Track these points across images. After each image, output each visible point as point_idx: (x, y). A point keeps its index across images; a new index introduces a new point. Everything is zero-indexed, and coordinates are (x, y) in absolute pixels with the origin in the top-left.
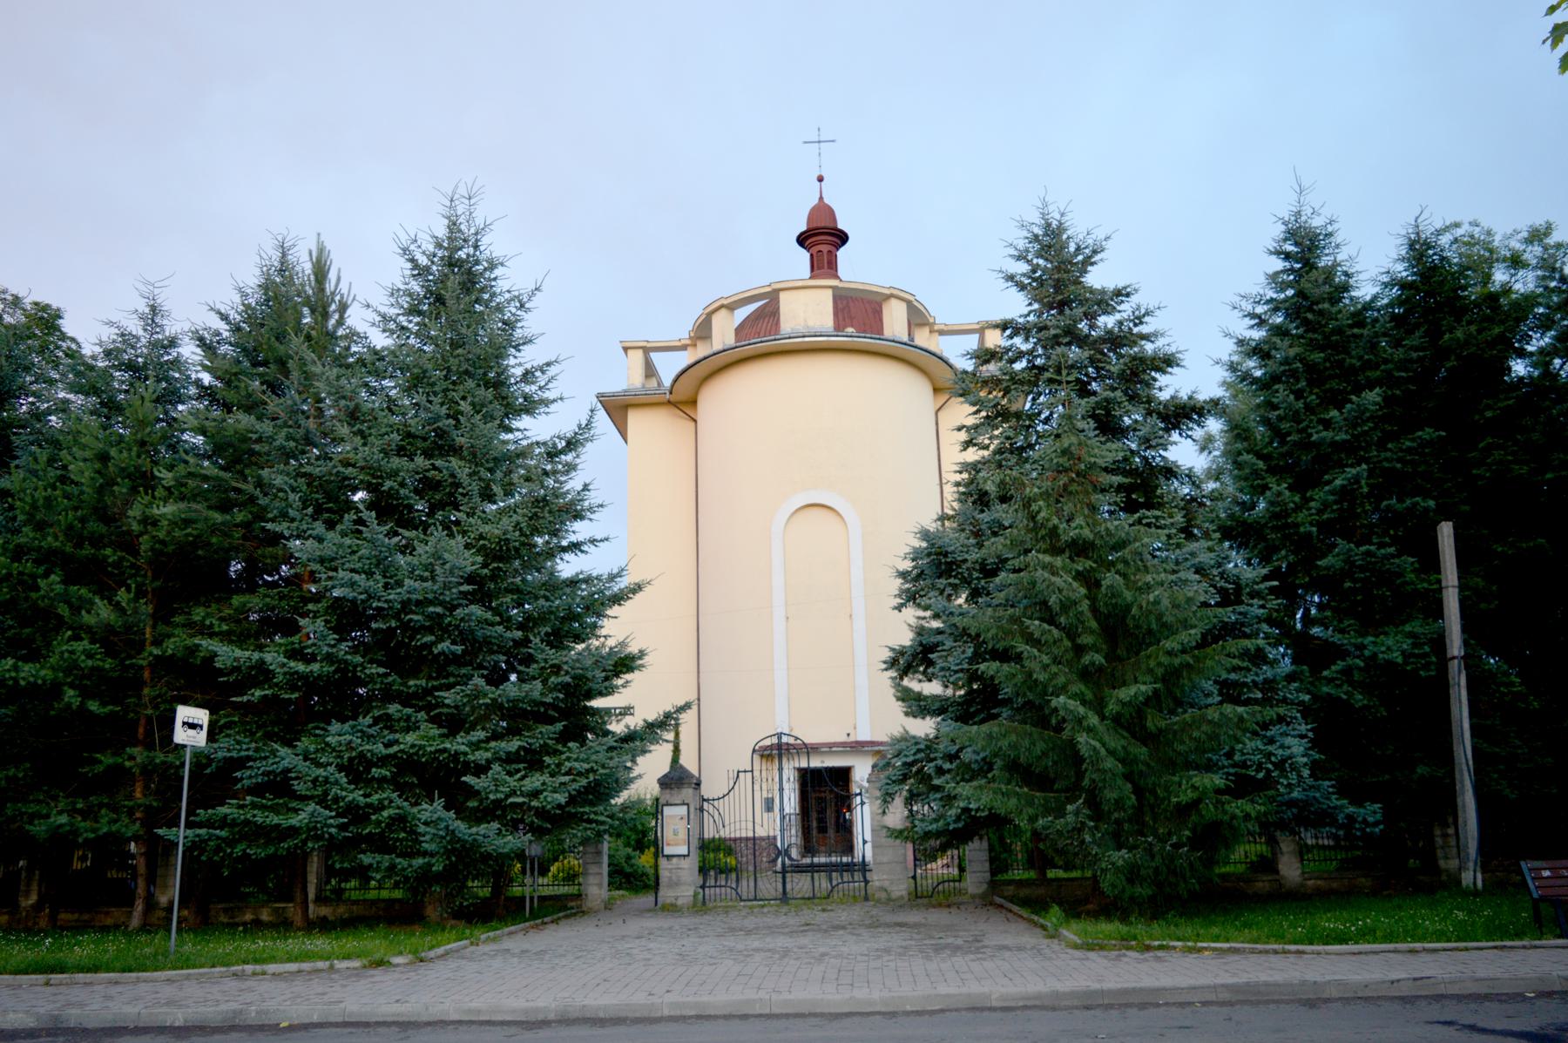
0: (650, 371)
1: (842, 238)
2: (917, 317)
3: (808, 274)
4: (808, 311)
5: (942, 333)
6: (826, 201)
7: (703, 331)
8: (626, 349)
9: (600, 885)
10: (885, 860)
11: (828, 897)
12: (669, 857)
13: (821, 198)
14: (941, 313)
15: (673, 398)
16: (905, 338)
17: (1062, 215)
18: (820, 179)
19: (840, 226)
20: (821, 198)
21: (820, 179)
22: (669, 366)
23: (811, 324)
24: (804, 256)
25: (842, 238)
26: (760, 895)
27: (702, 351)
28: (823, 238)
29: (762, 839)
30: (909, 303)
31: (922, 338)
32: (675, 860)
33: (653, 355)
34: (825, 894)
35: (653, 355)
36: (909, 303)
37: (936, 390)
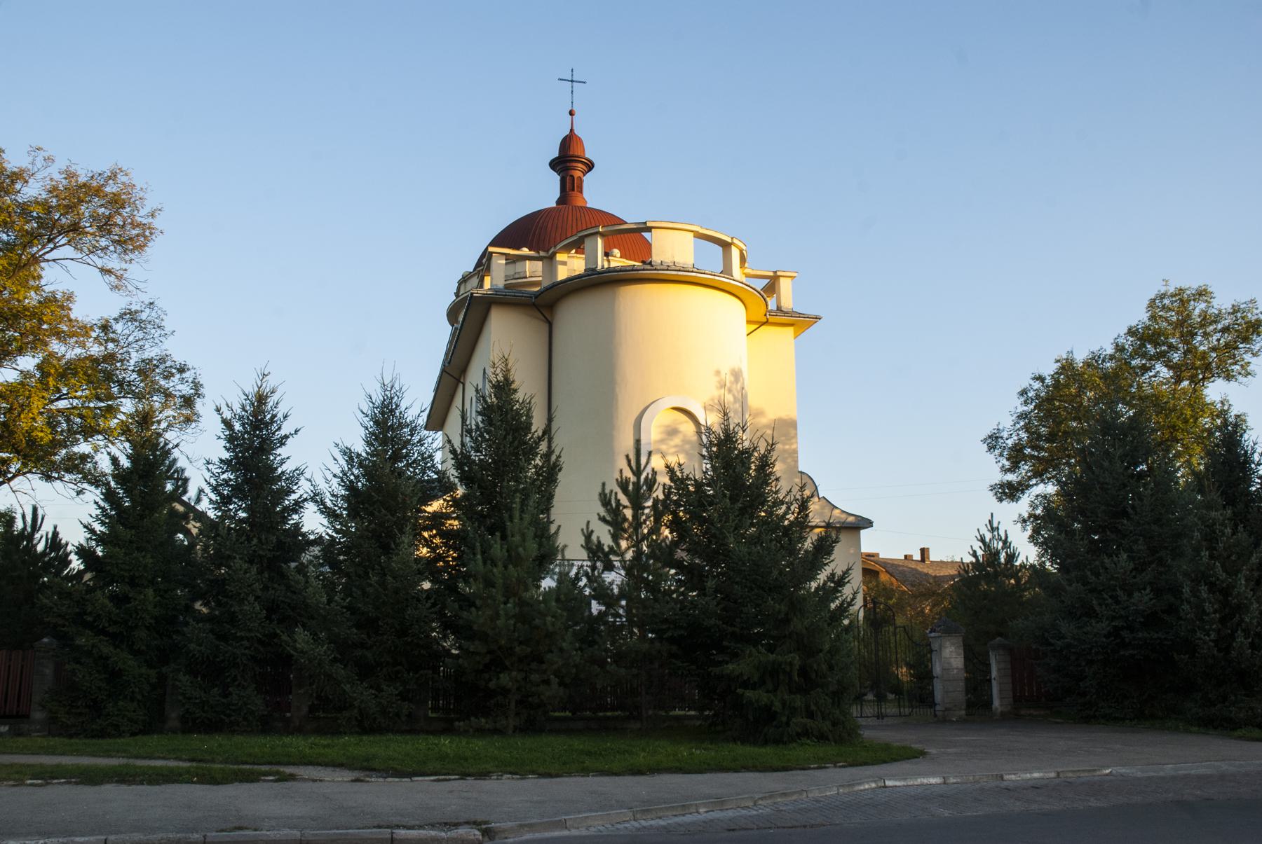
1: (590, 166)
13: (572, 130)
18: (571, 113)
20: (572, 130)
21: (571, 113)
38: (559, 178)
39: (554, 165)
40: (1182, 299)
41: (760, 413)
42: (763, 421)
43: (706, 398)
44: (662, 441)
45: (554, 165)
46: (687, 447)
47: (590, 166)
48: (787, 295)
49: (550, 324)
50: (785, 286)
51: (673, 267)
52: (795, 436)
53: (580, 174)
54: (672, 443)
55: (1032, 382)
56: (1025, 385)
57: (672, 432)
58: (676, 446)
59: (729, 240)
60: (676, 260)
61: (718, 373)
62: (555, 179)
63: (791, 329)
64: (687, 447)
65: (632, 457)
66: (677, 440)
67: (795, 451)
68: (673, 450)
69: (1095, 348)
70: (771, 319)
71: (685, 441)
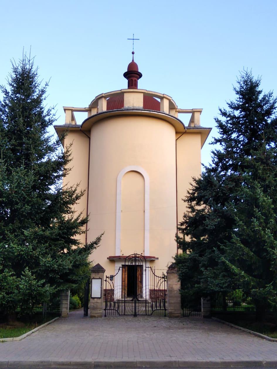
0: (73, 118)
1: (140, 75)
2: (172, 106)
3: (127, 88)
4: (134, 101)
5: (179, 112)
6: (135, 61)
7: (95, 104)
8: (65, 110)
9: (67, 308)
10: (173, 302)
11: (151, 315)
12: (94, 298)
13: (133, 60)
14: (180, 105)
15: (82, 129)
16: (168, 113)
17: (45, 99)
18: (133, 53)
19: (139, 71)
20: (133, 60)
21: (133, 53)
22: (81, 118)
23: (135, 105)
24: (126, 81)
25: (140, 75)
26: (126, 313)
27: (94, 112)
28: (132, 75)
29: (108, 290)
30: (170, 100)
31: (173, 113)
32: (96, 299)
33: (75, 113)
34: (150, 313)
35: (75, 113)
36: (170, 100)
37: (177, 133)
39: (126, 75)
45: (126, 75)
49: (90, 138)
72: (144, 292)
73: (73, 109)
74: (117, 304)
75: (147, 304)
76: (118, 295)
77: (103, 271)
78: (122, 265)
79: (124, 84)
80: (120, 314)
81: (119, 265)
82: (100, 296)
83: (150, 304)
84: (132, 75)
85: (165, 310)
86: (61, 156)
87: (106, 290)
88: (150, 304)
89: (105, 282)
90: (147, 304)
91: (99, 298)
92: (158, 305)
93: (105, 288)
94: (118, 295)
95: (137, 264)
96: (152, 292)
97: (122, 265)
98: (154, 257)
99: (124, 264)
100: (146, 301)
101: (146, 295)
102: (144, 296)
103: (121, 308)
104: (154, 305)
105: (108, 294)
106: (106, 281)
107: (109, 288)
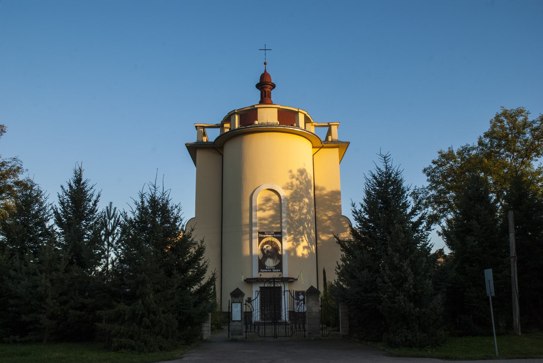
1: (273, 86)
7: (228, 119)
9: (208, 330)
13: (265, 71)
18: (265, 64)
20: (265, 71)
21: (265, 64)
22: (212, 135)
28: (265, 86)
32: (236, 322)
34: (290, 334)
38: (260, 92)
39: (259, 86)
40: (511, 116)
41: (323, 189)
42: (325, 192)
43: (284, 184)
44: (263, 204)
45: (259, 86)
46: (275, 206)
47: (273, 86)
48: (335, 135)
49: (222, 155)
50: (334, 129)
51: (268, 125)
52: (340, 199)
53: (269, 90)
54: (268, 205)
55: (432, 165)
56: (427, 166)
57: (268, 200)
58: (270, 206)
59: (297, 110)
60: (269, 121)
61: (291, 171)
62: (259, 92)
63: (337, 149)
64: (275, 206)
65: (109, 208)
66: (270, 204)
67: (340, 206)
68: (269, 208)
69: (464, 145)
70: (325, 145)
71: (274, 204)
72: (284, 315)
73: (205, 125)
74: (257, 327)
75: (287, 326)
76: (257, 317)
77: (242, 294)
78: (261, 288)
79: (255, 96)
80: (261, 335)
81: (256, 288)
82: (240, 319)
83: (289, 326)
84: (265, 86)
85: (305, 331)
86: (46, 278)
87: (246, 312)
88: (289, 326)
89: (245, 306)
90: (287, 326)
91: (239, 321)
92: (297, 326)
93: (244, 310)
94: (257, 317)
95: (276, 285)
96: (292, 314)
97: (261, 288)
98: (293, 278)
99: (263, 286)
100: (286, 322)
101: (285, 316)
102: (283, 318)
103: (261, 330)
104: (293, 327)
105: (247, 316)
106: (246, 304)
107: (248, 310)
